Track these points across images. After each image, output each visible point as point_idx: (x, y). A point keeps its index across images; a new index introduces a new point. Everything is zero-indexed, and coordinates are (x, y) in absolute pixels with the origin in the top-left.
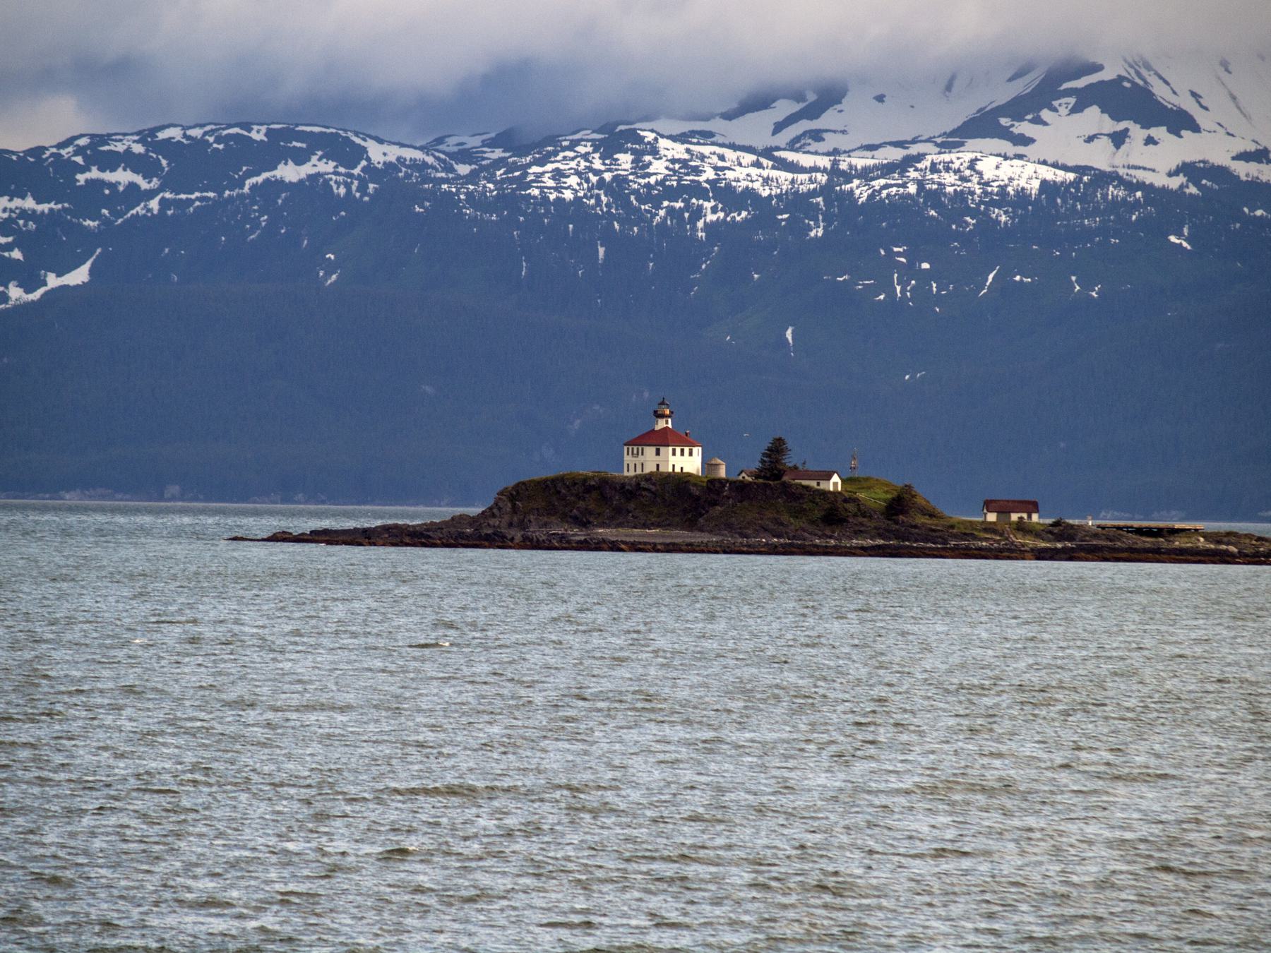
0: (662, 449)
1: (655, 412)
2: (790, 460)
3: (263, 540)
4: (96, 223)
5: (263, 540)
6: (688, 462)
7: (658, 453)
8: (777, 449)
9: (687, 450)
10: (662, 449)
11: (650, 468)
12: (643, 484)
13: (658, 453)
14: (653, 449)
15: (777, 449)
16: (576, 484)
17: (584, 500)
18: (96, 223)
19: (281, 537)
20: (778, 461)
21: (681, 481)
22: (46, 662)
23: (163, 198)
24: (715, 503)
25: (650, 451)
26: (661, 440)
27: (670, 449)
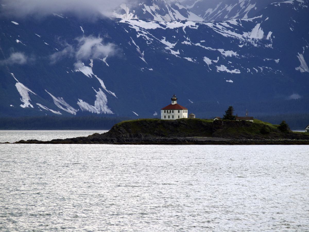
0: (180, 111)
1: (172, 99)
2: (234, 114)
3: (13, 143)
4: (303, 47)
5: (13, 143)
6: (185, 115)
7: (179, 112)
8: (230, 110)
9: (172, 111)
10: (180, 111)
11: (176, 118)
12: (182, 122)
13: (179, 112)
14: (177, 111)
15: (230, 110)
16: (151, 123)
17: (157, 127)
18: (303, 47)
19: (22, 142)
20: (231, 114)
21: (181, 122)
22: (148, 197)
23: (165, 28)
24: (219, 128)
25: (176, 112)
26: (172, 108)
27: (183, 110)
